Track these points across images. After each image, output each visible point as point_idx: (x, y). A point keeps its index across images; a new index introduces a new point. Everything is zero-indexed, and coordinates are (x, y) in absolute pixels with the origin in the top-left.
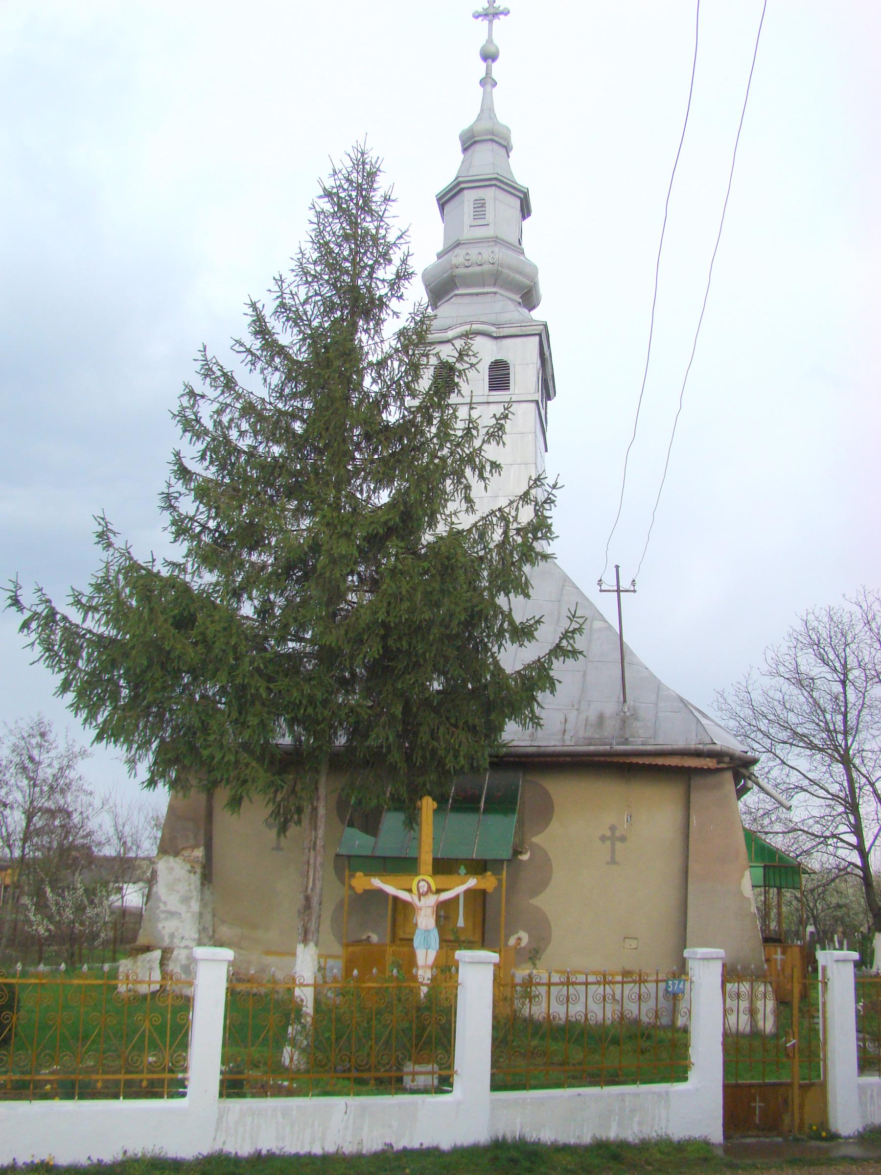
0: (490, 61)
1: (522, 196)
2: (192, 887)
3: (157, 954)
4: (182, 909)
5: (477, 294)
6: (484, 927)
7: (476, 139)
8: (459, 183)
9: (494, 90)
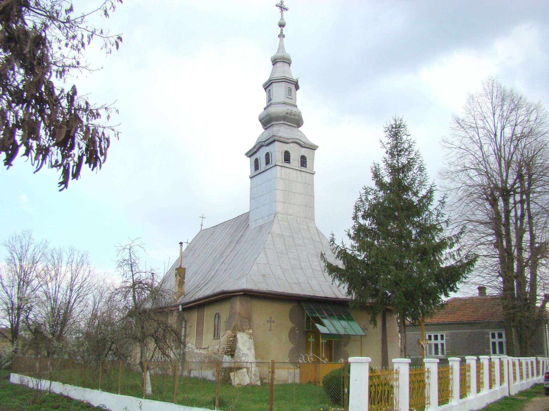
0: (282, 27)
2: (251, 344)
3: (245, 370)
4: (248, 352)
5: (290, 126)
6: (356, 362)
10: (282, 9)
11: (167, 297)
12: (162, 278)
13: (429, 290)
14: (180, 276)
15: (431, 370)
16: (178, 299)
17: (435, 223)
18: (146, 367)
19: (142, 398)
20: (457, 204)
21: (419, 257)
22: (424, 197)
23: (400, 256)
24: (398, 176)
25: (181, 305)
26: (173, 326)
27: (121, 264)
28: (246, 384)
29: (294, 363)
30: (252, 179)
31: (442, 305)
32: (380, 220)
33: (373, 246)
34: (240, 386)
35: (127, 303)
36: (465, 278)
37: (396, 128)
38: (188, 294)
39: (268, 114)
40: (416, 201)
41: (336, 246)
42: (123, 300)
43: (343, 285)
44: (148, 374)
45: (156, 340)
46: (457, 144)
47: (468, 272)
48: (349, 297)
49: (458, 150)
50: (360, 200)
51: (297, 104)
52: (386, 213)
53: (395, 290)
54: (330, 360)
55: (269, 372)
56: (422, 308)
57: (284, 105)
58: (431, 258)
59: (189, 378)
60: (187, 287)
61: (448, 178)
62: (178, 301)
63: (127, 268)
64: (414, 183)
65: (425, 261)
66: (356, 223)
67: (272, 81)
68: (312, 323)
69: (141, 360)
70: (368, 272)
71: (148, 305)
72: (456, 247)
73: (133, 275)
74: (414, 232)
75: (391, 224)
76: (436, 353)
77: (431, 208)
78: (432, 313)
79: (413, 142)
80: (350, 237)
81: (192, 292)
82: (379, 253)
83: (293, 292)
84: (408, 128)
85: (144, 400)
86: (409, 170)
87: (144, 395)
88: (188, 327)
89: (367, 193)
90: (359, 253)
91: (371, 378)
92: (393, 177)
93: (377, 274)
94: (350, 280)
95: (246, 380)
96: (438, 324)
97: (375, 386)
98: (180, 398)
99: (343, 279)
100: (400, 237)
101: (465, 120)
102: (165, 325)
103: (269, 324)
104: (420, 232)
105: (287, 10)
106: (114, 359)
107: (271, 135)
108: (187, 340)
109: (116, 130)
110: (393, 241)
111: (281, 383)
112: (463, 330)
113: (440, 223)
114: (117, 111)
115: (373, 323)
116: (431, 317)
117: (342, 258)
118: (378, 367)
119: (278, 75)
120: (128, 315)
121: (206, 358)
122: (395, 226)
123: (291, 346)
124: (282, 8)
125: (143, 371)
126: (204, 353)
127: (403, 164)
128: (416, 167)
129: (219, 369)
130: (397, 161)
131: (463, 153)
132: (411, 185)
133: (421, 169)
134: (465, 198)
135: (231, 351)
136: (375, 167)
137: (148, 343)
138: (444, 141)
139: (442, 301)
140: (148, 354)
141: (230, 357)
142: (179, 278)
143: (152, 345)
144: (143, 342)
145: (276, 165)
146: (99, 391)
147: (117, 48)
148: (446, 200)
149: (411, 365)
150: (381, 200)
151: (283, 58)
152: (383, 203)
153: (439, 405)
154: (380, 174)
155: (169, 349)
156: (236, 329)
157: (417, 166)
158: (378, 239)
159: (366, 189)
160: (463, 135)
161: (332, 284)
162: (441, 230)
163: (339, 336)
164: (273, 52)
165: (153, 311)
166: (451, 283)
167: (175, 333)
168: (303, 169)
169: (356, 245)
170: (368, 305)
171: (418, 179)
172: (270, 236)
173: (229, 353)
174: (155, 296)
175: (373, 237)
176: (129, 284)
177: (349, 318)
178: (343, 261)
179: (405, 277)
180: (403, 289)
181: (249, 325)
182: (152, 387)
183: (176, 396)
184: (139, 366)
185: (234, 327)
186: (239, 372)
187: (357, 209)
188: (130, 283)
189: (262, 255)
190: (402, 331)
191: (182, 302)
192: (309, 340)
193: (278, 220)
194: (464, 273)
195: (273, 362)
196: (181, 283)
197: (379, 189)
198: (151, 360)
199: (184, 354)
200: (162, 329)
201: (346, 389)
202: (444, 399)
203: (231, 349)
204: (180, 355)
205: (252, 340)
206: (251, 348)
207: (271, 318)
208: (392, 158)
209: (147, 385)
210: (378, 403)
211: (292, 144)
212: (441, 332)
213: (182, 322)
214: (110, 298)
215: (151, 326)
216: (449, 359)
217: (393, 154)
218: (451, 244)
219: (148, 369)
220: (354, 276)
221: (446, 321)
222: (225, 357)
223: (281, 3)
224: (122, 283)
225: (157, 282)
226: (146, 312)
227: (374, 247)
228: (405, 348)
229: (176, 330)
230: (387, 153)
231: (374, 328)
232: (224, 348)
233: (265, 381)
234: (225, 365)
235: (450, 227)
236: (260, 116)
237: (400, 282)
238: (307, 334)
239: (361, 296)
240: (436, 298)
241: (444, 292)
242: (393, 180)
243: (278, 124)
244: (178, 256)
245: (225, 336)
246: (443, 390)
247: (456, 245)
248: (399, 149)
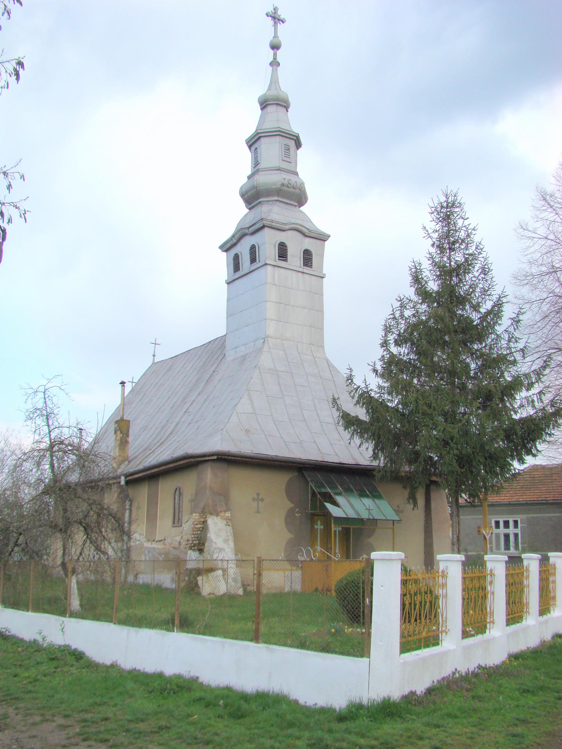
0: (275, 50)
1: (295, 138)
2: (229, 533)
3: (220, 572)
5: (287, 204)
7: (268, 103)
9: (278, 68)
10: (276, 21)
11: (102, 465)
12: (94, 436)
13: (495, 453)
14: (121, 432)
15: (496, 572)
16: (119, 467)
17: (505, 353)
18: (70, 569)
19: (66, 617)
20: (539, 324)
21: (479, 403)
22: (489, 313)
23: (452, 402)
24: (450, 282)
25: (124, 475)
26: (112, 507)
27: (32, 416)
28: (222, 593)
29: (292, 561)
31: (514, 475)
32: (422, 348)
33: (410, 387)
34: (212, 596)
35: (42, 474)
36: (550, 435)
37: (447, 207)
38: (134, 459)
39: (253, 186)
40: (477, 318)
41: (355, 387)
42: (34, 470)
43: (365, 445)
44: (74, 580)
45: (85, 529)
46: (542, 231)
47: (554, 426)
48: (375, 463)
49: (543, 242)
50: (392, 316)
51: (297, 170)
52: (431, 337)
53: (444, 453)
54: (348, 557)
55: (254, 574)
56: (484, 480)
57: (279, 172)
58: (498, 405)
59: (134, 586)
60: (132, 449)
61: (527, 284)
62: (119, 470)
63: (41, 421)
64: (474, 291)
65: (488, 410)
66: (385, 353)
68: (320, 501)
69: (64, 559)
70: (403, 426)
71: (74, 477)
72: (536, 389)
73: (50, 432)
74: (473, 366)
75: (439, 353)
76: (507, 547)
77: (499, 329)
78: (499, 488)
79: (474, 229)
80: (376, 374)
81: (141, 455)
82: (420, 397)
83: (292, 456)
84: (466, 208)
85: (69, 619)
86: (467, 271)
87: (68, 612)
88: (134, 509)
89: (403, 307)
90: (390, 398)
91: (404, 583)
92: (442, 283)
93: (416, 428)
94: (376, 437)
95: (222, 588)
96: (510, 504)
97: (411, 595)
98: (121, 615)
99: (366, 436)
100: (452, 373)
101: (556, 195)
102: (99, 507)
103: (255, 504)
104: (483, 365)
105: (283, 22)
106: (22, 559)
107: (259, 218)
108: (133, 527)
109: (21, 208)
110: (442, 379)
111: (274, 591)
112: (548, 513)
113: (512, 353)
114: (23, 177)
115: (411, 501)
116: (497, 494)
117: (363, 404)
118: (417, 567)
119: (269, 126)
120: (43, 493)
121: (160, 554)
122: (444, 357)
123: (289, 536)
124: (276, 18)
125: (66, 575)
126: (158, 548)
127: (458, 263)
128: (477, 268)
129: (180, 570)
130: (449, 258)
131: (550, 246)
132: (469, 295)
133: (485, 271)
134: (552, 315)
136: (416, 268)
137: (74, 534)
138: (522, 228)
139: (515, 469)
140: (73, 550)
141: (197, 552)
142: (120, 435)
143: (80, 536)
144: (66, 532)
145: (266, 264)
147: (18, 79)
148: (521, 317)
149: (465, 564)
150: (424, 318)
152: (427, 321)
153: (507, 625)
154: (422, 278)
155: (106, 542)
156: (205, 512)
157: (478, 265)
158: (419, 376)
159: (401, 301)
160: (552, 219)
161: (350, 443)
162: (514, 362)
163: (361, 521)
164: (261, 89)
165: (81, 485)
166: (528, 443)
167: (114, 518)
168: (307, 270)
169: (386, 385)
170: (403, 474)
171: (481, 286)
172: (257, 371)
173: (196, 548)
174: (84, 462)
175: (411, 373)
176: (43, 446)
177: (375, 495)
178: (366, 409)
179: (459, 433)
180: (456, 452)
181: (226, 504)
182: (81, 600)
183: (116, 612)
184: (60, 568)
185: (204, 508)
186: (211, 575)
187: (387, 330)
188: (45, 444)
190: (455, 514)
191: (125, 472)
193: (269, 348)
194: (549, 427)
195: (260, 560)
196: (123, 443)
197: (420, 301)
198: (78, 559)
199: (129, 550)
200: (95, 512)
201: (367, 600)
202: (515, 615)
203: (199, 541)
204: (122, 551)
205: (231, 527)
207: (258, 494)
208: (440, 254)
209: (72, 597)
210: (416, 620)
211: (290, 232)
212: (513, 516)
213: (125, 502)
214: (16, 466)
215: (78, 508)
216: (523, 556)
217: (442, 247)
218: (528, 384)
219: (74, 572)
220: (382, 433)
221: (522, 499)
222: (190, 553)
223: (273, 11)
224: (34, 443)
225: (86, 441)
226: (70, 487)
227: (412, 389)
228: (458, 540)
229: (116, 514)
230: (433, 245)
231: (413, 509)
232: (188, 541)
233: (249, 588)
234: (191, 565)
235: (527, 360)
236: (241, 188)
237: (450, 441)
238: (312, 518)
239: (392, 461)
240: (505, 467)
241: (517, 455)
242: (442, 287)
243: (269, 201)
244: (118, 402)
245: (190, 522)
246: (514, 603)
247: (536, 385)
248: (452, 239)
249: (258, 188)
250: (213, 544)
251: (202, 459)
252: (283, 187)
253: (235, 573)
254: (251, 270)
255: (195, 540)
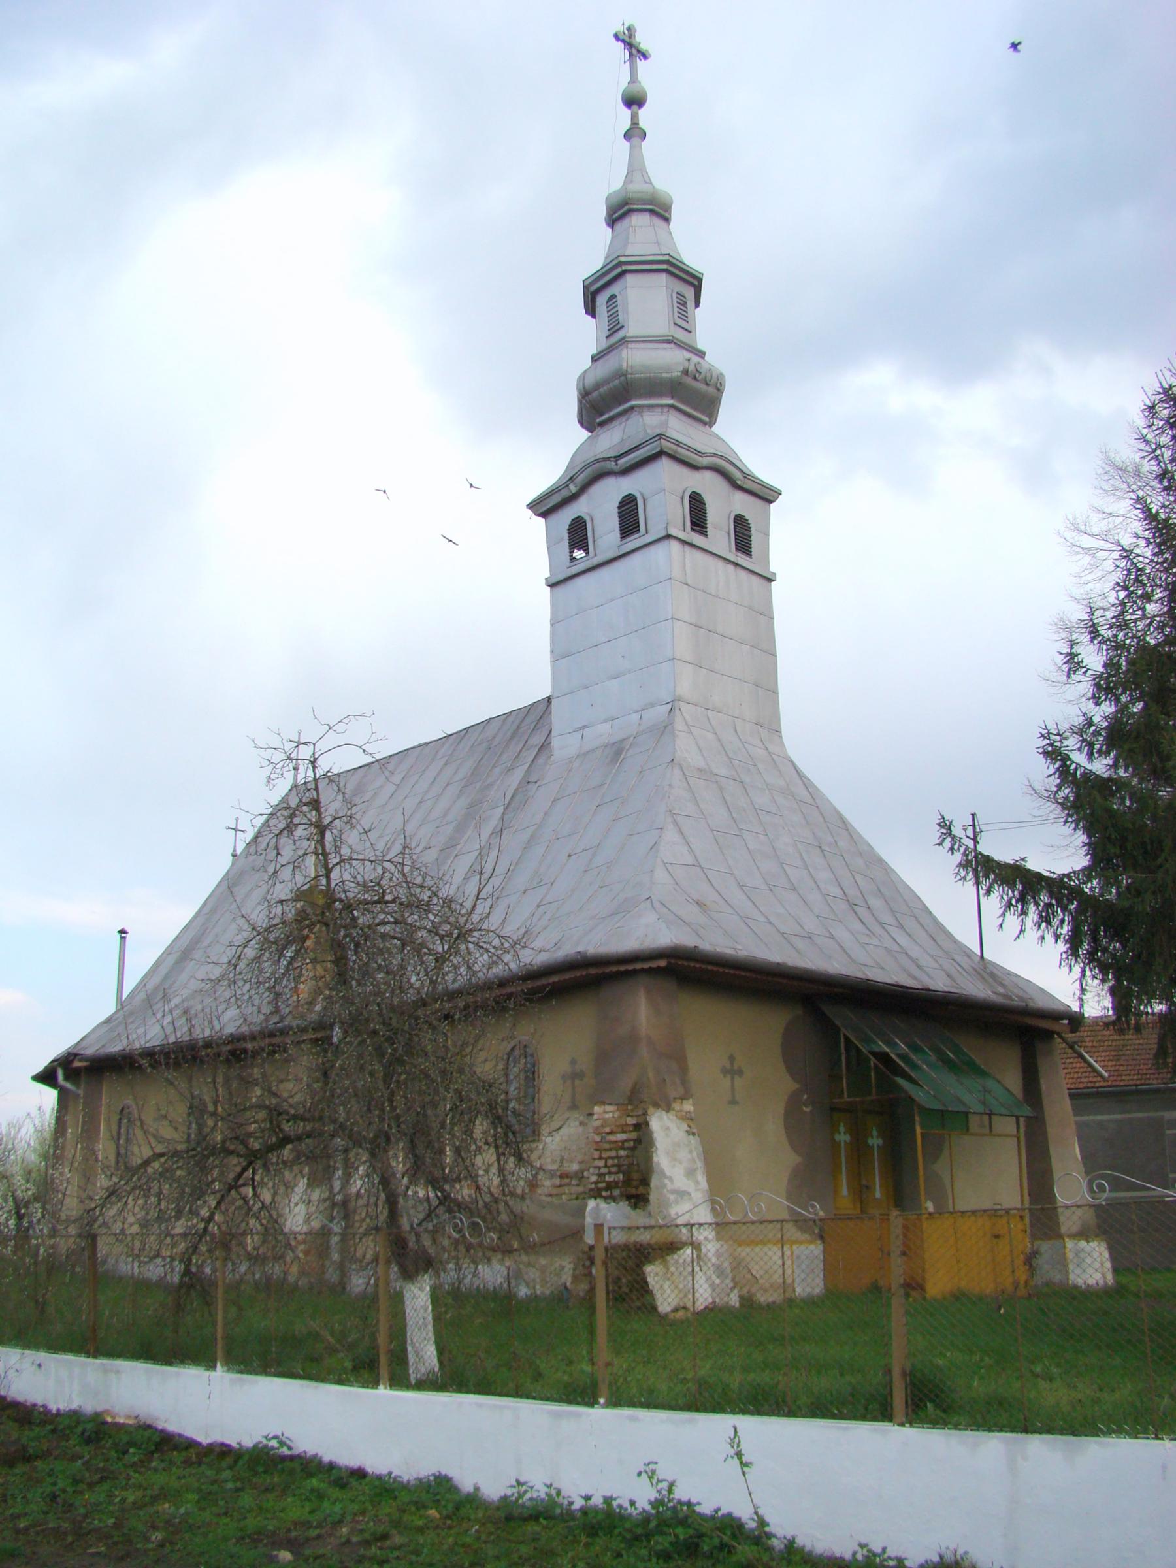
0: (635, 107)
1: (665, 266)
2: (695, 1154)
6: (952, 1176)
8: (620, 264)
9: (644, 144)
10: (634, 52)
28: (700, 1305)
30: (560, 590)
34: (680, 1314)
57: (672, 345)
67: (624, 268)
103: (727, 1082)
135: (628, 1182)
146: (220, 1375)
151: (652, 201)
189: (671, 835)
192: (837, 1137)
206: (695, 1170)
207: (732, 1058)
211: (708, 475)
249: (629, 376)
250: (666, 1181)
251: (622, 968)
252: (686, 377)
253: (718, 1255)
254: (622, 552)
255: (610, 1173)
